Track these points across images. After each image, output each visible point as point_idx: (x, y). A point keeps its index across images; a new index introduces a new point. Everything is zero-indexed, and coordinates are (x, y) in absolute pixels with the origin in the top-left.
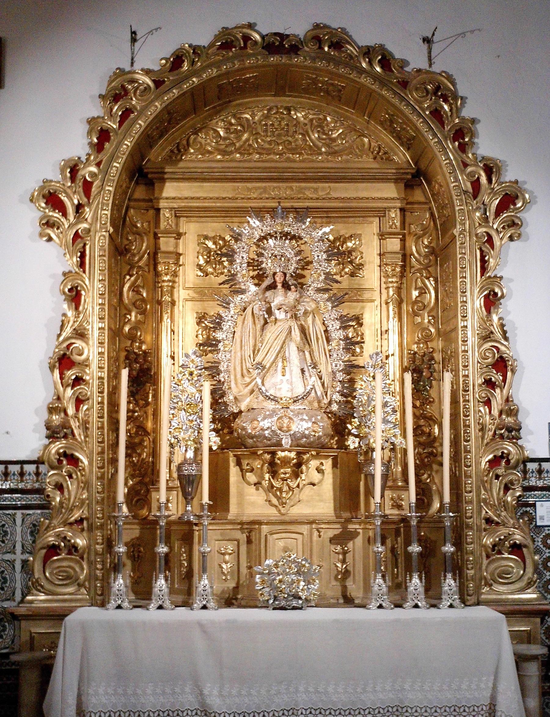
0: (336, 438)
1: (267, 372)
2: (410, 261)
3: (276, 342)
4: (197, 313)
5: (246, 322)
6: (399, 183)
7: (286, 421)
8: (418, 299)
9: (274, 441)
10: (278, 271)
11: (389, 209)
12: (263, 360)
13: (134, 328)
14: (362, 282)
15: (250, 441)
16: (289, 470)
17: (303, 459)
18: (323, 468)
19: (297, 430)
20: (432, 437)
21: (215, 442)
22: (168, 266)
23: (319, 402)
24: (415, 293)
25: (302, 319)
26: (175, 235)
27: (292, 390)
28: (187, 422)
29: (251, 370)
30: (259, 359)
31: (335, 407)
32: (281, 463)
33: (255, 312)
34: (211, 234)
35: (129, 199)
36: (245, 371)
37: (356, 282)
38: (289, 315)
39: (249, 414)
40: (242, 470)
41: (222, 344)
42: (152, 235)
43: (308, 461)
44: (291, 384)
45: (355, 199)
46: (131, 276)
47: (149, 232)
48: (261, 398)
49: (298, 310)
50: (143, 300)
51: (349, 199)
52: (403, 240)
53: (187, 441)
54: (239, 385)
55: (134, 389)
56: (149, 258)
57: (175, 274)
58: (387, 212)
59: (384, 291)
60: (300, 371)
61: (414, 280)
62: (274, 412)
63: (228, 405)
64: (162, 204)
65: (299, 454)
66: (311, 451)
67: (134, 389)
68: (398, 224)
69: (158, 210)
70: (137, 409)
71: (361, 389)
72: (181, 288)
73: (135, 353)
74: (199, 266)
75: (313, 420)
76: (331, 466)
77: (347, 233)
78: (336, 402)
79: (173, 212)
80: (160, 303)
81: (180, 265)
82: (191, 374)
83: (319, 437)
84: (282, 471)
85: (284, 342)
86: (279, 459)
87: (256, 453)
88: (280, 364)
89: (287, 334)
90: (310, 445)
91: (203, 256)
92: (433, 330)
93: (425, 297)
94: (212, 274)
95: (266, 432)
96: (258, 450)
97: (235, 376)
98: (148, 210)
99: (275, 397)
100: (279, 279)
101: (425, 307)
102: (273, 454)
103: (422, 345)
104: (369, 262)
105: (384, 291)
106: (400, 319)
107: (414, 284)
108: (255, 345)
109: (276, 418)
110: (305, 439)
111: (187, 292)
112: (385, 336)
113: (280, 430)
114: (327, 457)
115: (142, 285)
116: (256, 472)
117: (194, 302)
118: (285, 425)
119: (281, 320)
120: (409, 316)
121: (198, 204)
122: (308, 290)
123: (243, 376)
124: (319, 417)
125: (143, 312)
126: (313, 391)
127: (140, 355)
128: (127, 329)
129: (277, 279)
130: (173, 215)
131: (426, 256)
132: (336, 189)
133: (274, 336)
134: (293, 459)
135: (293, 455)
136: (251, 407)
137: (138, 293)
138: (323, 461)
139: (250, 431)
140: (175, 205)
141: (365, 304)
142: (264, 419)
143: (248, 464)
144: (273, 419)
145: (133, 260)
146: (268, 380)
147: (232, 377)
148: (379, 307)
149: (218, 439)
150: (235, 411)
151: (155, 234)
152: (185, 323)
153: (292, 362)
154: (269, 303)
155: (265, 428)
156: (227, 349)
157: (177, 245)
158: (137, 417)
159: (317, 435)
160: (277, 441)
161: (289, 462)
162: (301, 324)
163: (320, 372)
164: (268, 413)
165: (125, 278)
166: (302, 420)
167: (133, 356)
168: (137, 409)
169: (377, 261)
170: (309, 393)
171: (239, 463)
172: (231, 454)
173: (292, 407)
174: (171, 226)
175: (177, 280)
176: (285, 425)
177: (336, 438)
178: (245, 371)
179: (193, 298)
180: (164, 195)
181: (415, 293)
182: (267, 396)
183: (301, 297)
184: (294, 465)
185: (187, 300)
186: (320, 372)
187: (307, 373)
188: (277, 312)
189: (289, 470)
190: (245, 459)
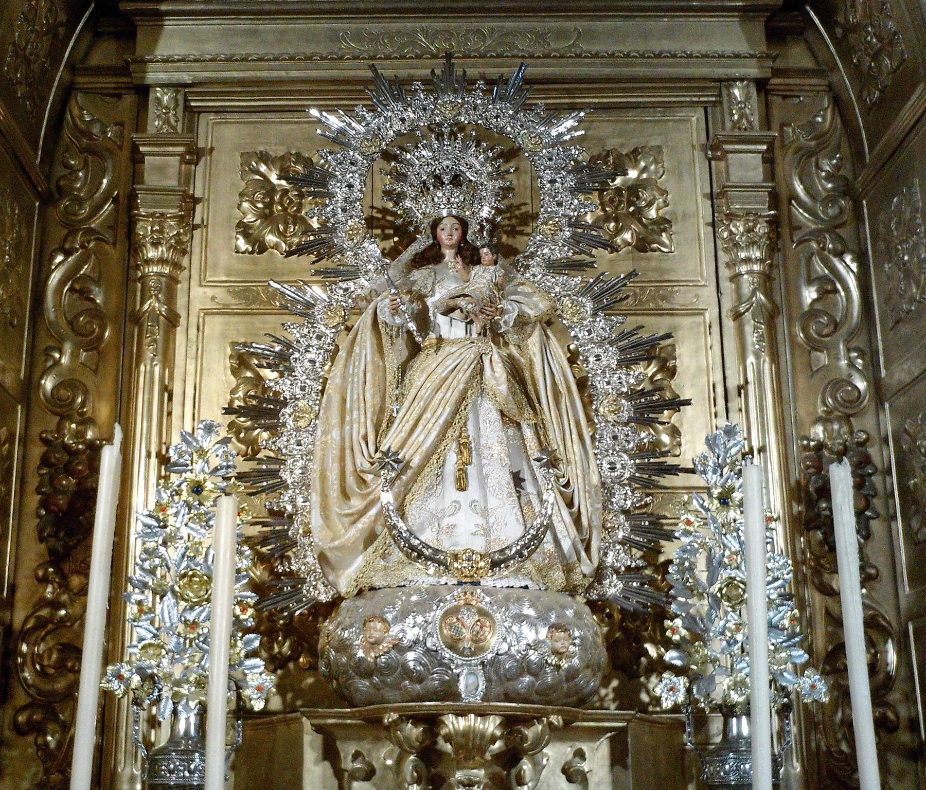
0: (615, 683)
1: (414, 480)
2: (790, 211)
3: (440, 395)
4: (234, 344)
5: (357, 349)
6: (752, 19)
7: (469, 619)
8: (818, 306)
9: (434, 681)
10: (445, 213)
11: (730, 81)
12: (402, 447)
13: (68, 384)
14: (665, 265)
15: (363, 684)
16: (480, 774)
17: (524, 738)
18: (585, 766)
19: (504, 647)
20: (881, 676)
21: (259, 689)
22: (160, 224)
23: (568, 570)
24: (810, 295)
25: (512, 338)
26: (181, 149)
27: (487, 532)
28: (181, 628)
29: (369, 477)
30: (391, 441)
31: (613, 588)
32: (456, 751)
33: (380, 317)
34: (278, 151)
35: (71, 67)
36: (351, 480)
37: (653, 264)
38: (476, 328)
39: (360, 602)
40: (338, 773)
41: (288, 410)
42: (126, 153)
43: (538, 744)
44: (485, 513)
45: (642, 56)
46: (68, 254)
47: (121, 148)
48: (397, 555)
49: (503, 312)
50: (97, 314)
51: (628, 56)
52: (769, 160)
53: (178, 683)
54: (335, 519)
55: (59, 546)
56: (116, 211)
57: (181, 248)
58: (724, 92)
59: (727, 286)
60: (508, 478)
61: (803, 262)
62: (433, 596)
63: (303, 581)
64: (154, 75)
65: (511, 723)
66: (547, 714)
67: (59, 546)
68: (755, 119)
69: (143, 91)
70: (64, 598)
71: (687, 533)
72: (194, 283)
73: (66, 448)
74: (244, 229)
75: (553, 619)
76: (607, 762)
77: (622, 145)
78: (617, 571)
79: (180, 98)
80: (136, 319)
81: (195, 227)
82: (197, 489)
83: (572, 674)
84: (459, 775)
85: (463, 398)
86: (448, 738)
87: (379, 721)
88: (452, 459)
89: (472, 377)
90: (545, 695)
91: (253, 203)
92: (861, 385)
93: (836, 304)
94: (276, 246)
95: (410, 656)
96: (386, 710)
97: (324, 496)
98: (119, 96)
99: (436, 551)
100: (448, 235)
101: (836, 326)
102: (432, 722)
103: (836, 427)
104: (685, 216)
105: (727, 286)
106: (775, 358)
107: (803, 270)
108: (382, 410)
109: (439, 613)
110: (527, 679)
111: (210, 292)
112: (735, 403)
113: (452, 647)
114: (594, 734)
115: (95, 275)
116: (383, 777)
117: (227, 318)
118: (467, 634)
119: (453, 342)
120: (797, 352)
121: (241, 75)
122: (527, 267)
123: (345, 495)
124: (570, 613)
125: (94, 345)
126: (548, 537)
127: (77, 453)
128: (48, 383)
129: (443, 236)
130: (181, 102)
131: (830, 199)
132: (591, 35)
133: (436, 378)
134: (493, 739)
135: (491, 726)
136: (365, 582)
137: (84, 294)
138: (585, 747)
139: (360, 654)
140: (187, 78)
141: (678, 320)
142: (402, 617)
143: (356, 756)
144: (430, 616)
145: (75, 215)
146: (416, 503)
147: (315, 498)
148: (716, 329)
149: (269, 680)
150: (323, 598)
151: (135, 148)
152: (200, 372)
153: (486, 452)
154: (421, 298)
155: (405, 642)
156: (302, 423)
157: (187, 179)
158: (62, 620)
159: (565, 664)
160: (443, 682)
161: (482, 750)
162: (510, 357)
163: (567, 485)
164: (414, 598)
165: (52, 258)
166: (520, 618)
167: (60, 456)
168: (64, 598)
169: (704, 209)
170: (537, 539)
171: (330, 754)
172: (307, 723)
173: (488, 582)
174: (174, 128)
175: (185, 262)
176: (467, 634)
177: (615, 683)
178: (351, 480)
179: (226, 306)
180: (162, 51)
181: (810, 295)
182: (413, 548)
183: (508, 278)
184: (497, 757)
185: (208, 313)
186: (567, 485)
187: (529, 487)
188: (442, 320)
189: (482, 772)
190: (347, 738)
